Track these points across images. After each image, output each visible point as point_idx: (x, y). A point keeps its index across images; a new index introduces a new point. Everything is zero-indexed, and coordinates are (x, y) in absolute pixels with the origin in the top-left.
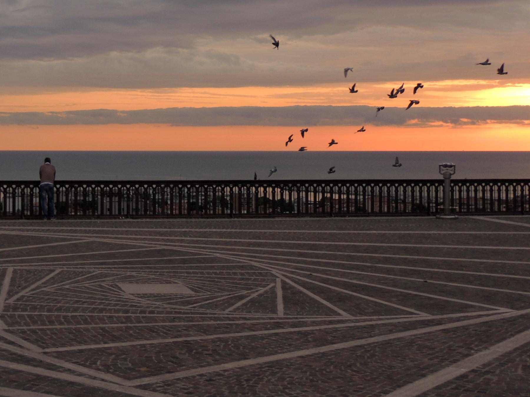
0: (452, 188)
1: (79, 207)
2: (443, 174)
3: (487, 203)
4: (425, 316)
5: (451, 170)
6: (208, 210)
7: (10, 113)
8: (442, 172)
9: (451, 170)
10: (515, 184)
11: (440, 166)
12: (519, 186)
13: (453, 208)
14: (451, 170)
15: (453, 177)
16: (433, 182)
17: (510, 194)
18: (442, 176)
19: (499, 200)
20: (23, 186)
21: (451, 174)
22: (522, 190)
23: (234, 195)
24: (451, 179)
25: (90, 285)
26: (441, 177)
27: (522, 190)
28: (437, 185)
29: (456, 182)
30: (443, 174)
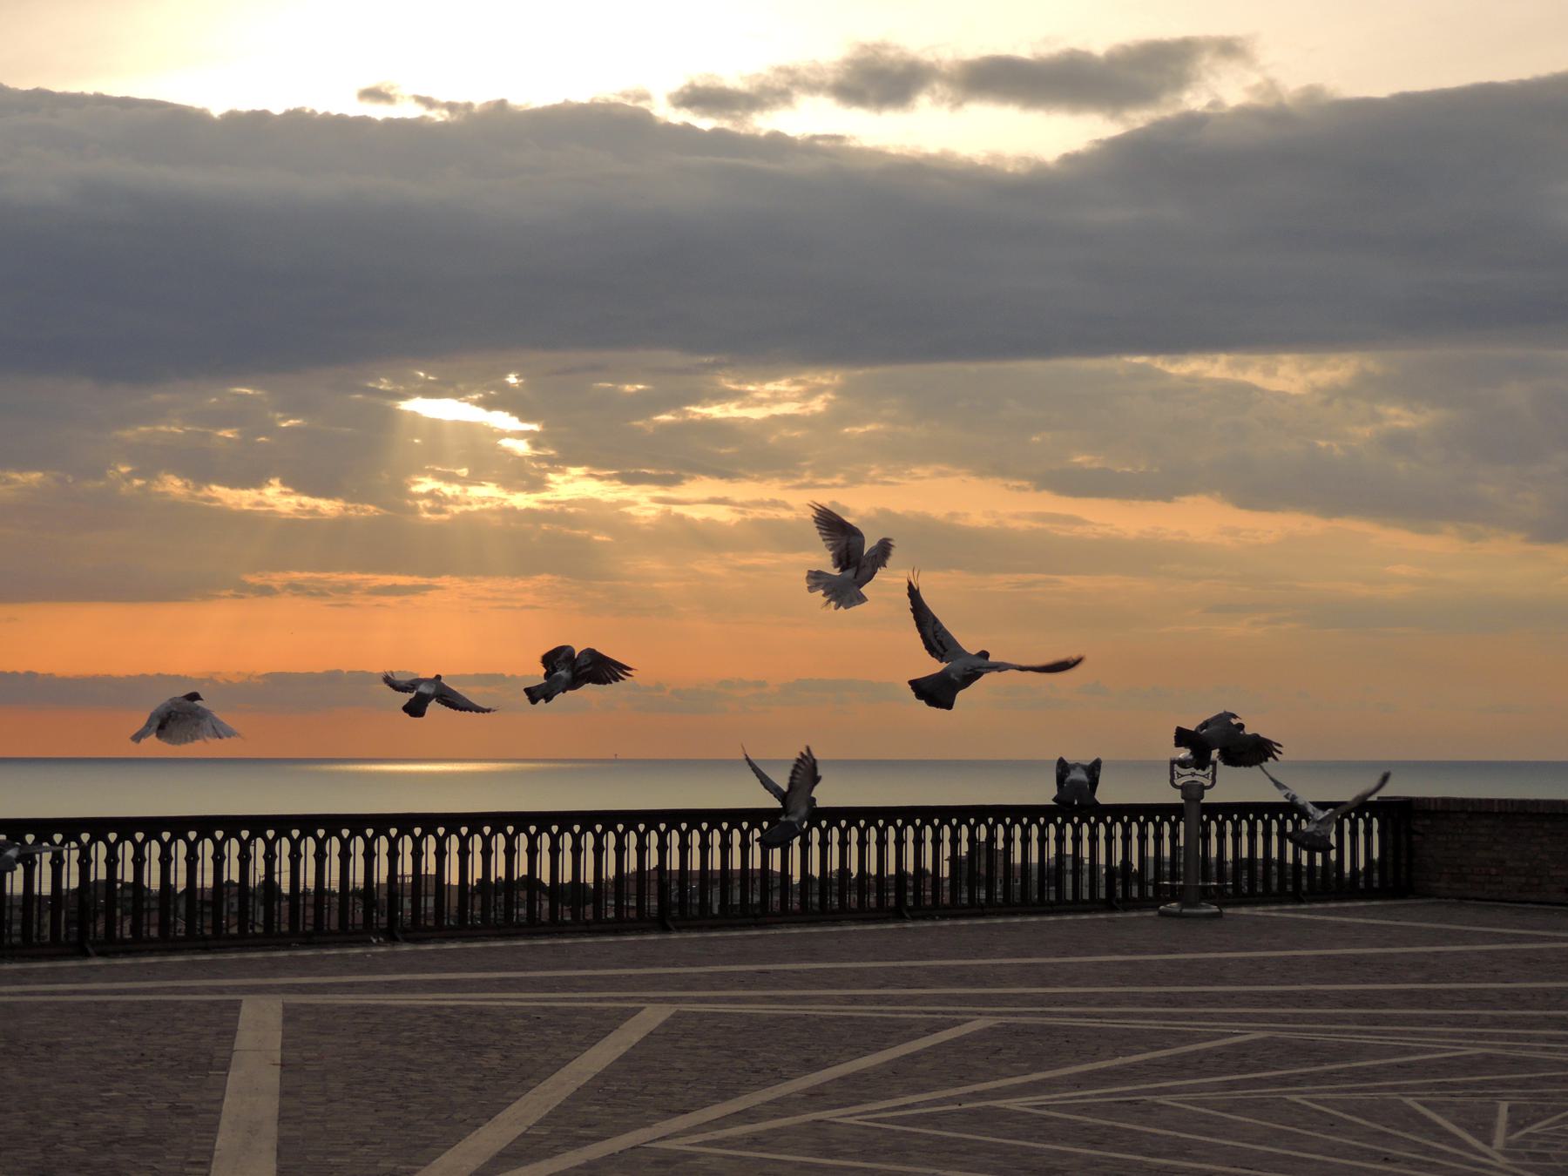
0: (1206, 825)
1: (375, 937)
2: (1182, 787)
3: (149, 910)
4: (1014, 1104)
5: (1206, 776)
6: (1376, 885)
7: (451, 107)
8: (1179, 782)
9: (1204, 776)
10: (112, 837)
11: (1173, 762)
12: (208, 842)
13: (1173, 883)
14: (1204, 776)
15: (1210, 797)
16: (1150, 811)
17: (979, 854)
18: (1179, 791)
19: (531, 879)
20: (321, 833)
21: (1203, 787)
22: (112, 861)
23: (429, 877)
24: (1202, 801)
25: (691, 1145)
26: (1176, 797)
27: (112, 861)
28: (441, 831)
29: (1213, 810)
30: (1182, 787)
